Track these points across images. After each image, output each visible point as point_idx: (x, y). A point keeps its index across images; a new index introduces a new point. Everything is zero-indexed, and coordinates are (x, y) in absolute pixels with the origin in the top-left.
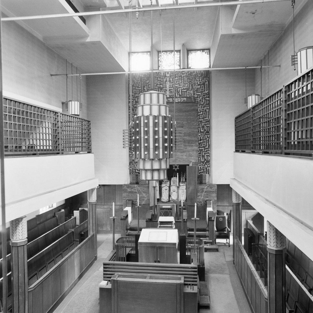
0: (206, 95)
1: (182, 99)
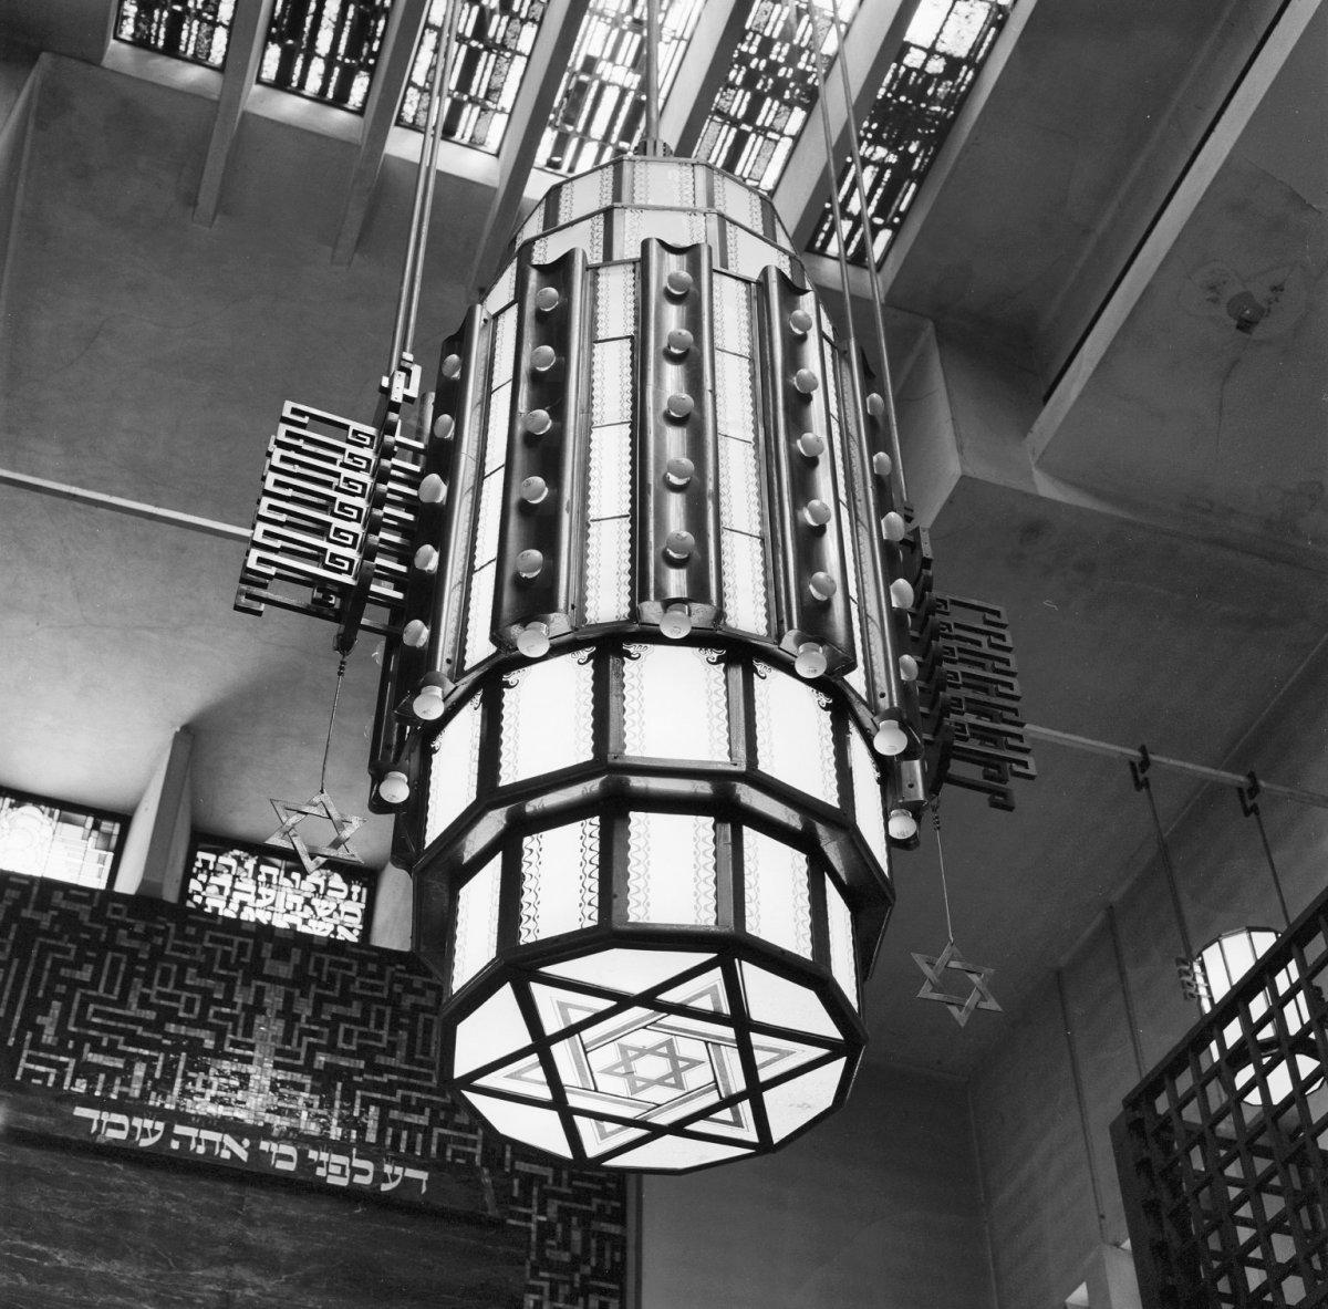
0: (598, 1194)
1: (388, 1169)
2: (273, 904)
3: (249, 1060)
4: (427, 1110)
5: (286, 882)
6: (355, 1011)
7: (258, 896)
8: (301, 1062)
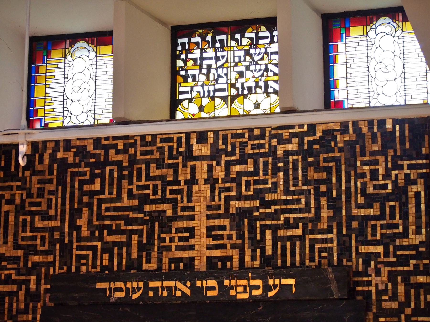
0: (412, 257)
2: (227, 62)
4: (301, 225)
5: (233, 43)
7: (217, 59)
8: (221, 212)
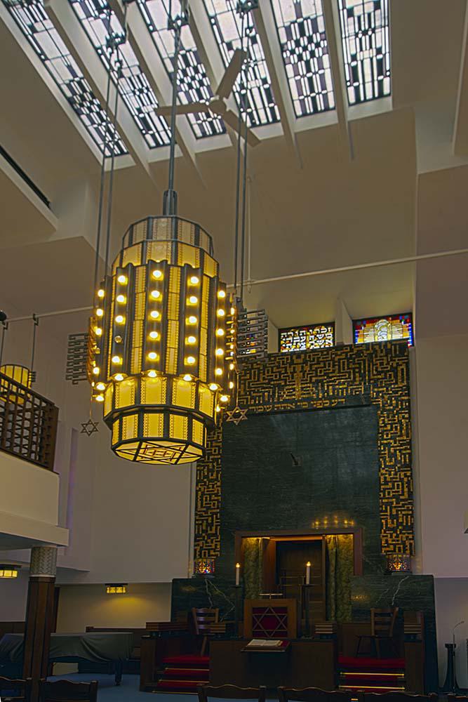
1: (333, 401)
3: (294, 385)
6: (322, 365)
